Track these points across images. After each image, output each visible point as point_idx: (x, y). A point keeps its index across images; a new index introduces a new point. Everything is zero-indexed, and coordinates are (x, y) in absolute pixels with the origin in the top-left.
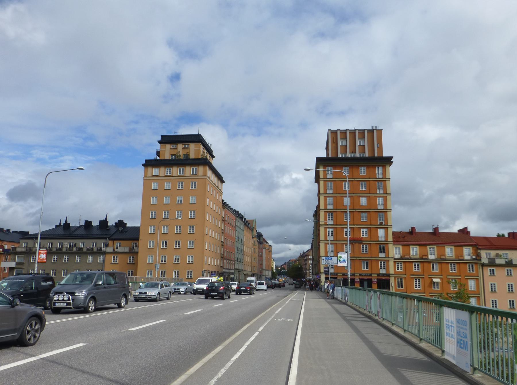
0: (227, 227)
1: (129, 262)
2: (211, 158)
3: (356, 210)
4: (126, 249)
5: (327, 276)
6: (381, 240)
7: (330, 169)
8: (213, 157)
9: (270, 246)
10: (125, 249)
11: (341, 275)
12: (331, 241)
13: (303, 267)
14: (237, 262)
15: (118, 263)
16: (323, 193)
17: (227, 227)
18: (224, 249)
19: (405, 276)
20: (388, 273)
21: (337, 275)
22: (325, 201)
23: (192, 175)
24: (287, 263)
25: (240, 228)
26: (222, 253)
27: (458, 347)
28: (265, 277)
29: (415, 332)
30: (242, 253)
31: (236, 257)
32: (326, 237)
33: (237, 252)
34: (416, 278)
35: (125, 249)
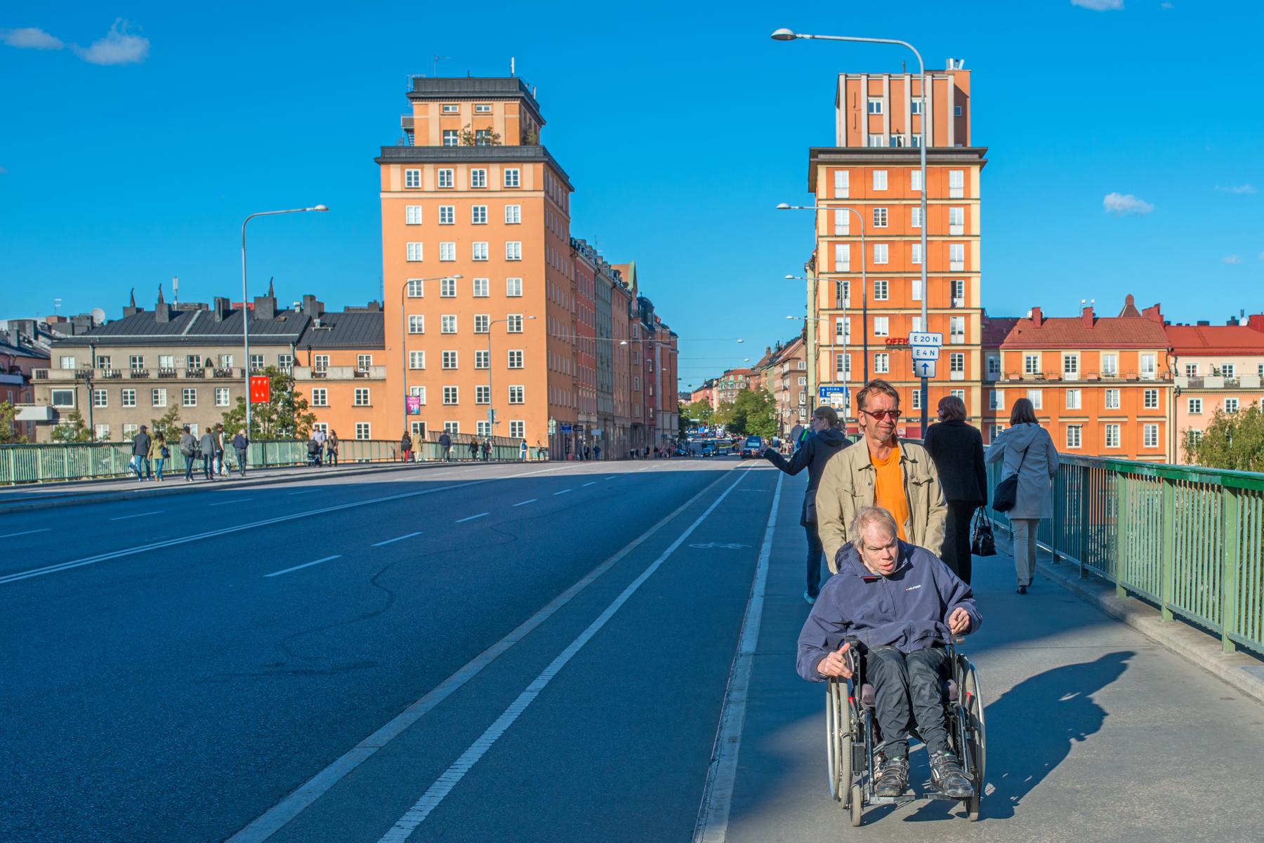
1: (356, 404)
3: (900, 240)
4: (345, 371)
7: (842, 178)
9: (672, 334)
10: (342, 372)
12: (847, 346)
13: (777, 397)
15: (372, 406)
18: (577, 366)
22: (832, 252)
23: (507, 189)
24: (715, 382)
25: (604, 300)
26: (575, 375)
30: (610, 369)
34: (1109, 424)
35: (342, 372)
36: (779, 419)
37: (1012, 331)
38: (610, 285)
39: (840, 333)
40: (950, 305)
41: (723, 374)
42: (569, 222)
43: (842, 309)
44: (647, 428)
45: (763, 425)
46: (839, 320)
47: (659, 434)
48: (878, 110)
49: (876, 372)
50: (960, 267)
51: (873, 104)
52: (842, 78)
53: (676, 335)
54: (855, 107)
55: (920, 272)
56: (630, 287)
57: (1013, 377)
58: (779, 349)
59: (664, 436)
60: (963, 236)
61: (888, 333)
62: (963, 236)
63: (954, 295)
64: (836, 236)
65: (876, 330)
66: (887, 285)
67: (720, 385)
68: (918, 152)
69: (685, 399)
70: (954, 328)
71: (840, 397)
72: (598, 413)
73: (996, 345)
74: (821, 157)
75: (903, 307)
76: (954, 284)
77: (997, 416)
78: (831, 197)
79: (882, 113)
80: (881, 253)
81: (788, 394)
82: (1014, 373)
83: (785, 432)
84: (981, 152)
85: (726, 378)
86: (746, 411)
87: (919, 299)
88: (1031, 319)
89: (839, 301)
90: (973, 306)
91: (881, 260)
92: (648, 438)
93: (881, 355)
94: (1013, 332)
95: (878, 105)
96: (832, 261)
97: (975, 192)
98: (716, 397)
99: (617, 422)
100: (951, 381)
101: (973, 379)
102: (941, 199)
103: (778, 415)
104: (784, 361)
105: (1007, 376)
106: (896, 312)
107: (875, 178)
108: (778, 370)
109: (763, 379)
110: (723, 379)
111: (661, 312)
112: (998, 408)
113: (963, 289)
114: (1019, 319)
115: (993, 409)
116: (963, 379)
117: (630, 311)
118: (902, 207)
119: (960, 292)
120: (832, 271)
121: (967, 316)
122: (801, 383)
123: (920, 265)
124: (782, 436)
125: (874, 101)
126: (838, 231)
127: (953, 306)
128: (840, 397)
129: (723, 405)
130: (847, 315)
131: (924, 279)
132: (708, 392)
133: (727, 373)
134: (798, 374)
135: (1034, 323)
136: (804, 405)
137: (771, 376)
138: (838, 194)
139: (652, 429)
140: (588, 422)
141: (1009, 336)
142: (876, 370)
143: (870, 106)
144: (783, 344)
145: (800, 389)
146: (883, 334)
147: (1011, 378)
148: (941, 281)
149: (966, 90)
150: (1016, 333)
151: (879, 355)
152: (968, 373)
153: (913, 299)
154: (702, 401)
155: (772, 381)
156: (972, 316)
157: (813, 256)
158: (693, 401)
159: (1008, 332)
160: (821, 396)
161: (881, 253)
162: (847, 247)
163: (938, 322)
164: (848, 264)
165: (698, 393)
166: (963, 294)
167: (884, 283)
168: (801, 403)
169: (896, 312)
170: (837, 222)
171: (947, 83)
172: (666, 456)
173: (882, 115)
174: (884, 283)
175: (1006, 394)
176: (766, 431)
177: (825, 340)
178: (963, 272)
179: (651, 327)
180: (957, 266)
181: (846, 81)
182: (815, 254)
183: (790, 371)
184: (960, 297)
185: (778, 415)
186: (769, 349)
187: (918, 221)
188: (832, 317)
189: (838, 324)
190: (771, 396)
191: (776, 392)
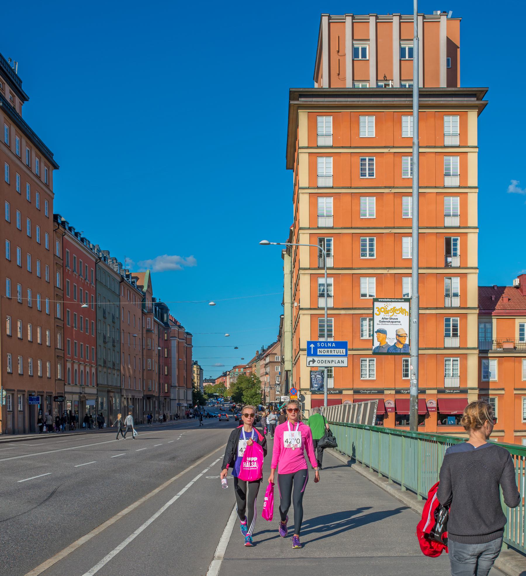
0: (90, 295)
2: (17, 100)
5: (317, 397)
6: (450, 346)
8: (24, 98)
9: (188, 333)
11: (351, 392)
12: (329, 309)
13: (261, 379)
14: (105, 370)
16: (307, 185)
17: (90, 295)
19: (503, 392)
20: (462, 387)
21: (340, 392)
24: (228, 373)
25: (110, 289)
27: (170, 315)
28: (177, 402)
29: (429, 445)
30: (117, 349)
31: (99, 356)
32: (313, 299)
33: (102, 345)
36: (263, 393)
37: (501, 299)
38: (119, 279)
39: (322, 295)
40: (443, 265)
41: (233, 368)
42: (53, 198)
43: (323, 268)
44: (162, 399)
45: (252, 397)
46: (321, 281)
47: (174, 404)
48: (364, 55)
49: (362, 338)
50: (455, 222)
51: (358, 49)
52: (325, 20)
53: (191, 335)
54: (338, 52)
55: (411, 228)
56: (145, 289)
57: (507, 346)
58: (264, 351)
59: (179, 404)
60: (459, 187)
61: (375, 294)
62: (459, 187)
63: (448, 253)
64: (318, 188)
65: (363, 292)
66: (375, 242)
67: (231, 374)
68: (409, 95)
69: (213, 383)
70: (447, 290)
71: (402, 311)
72: (97, 385)
73: (487, 311)
74: (302, 100)
75: (392, 266)
76: (448, 242)
77: (490, 388)
78: (313, 145)
79: (368, 58)
80: (367, 207)
81: (268, 376)
82: (508, 341)
83: (266, 402)
84: (478, 94)
85: (234, 370)
86: (242, 388)
87: (410, 257)
88: (517, 287)
89: (321, 260)
90: (469, 265)
91: (367, 215)
92: (163, 406)
93: (368, 319)
94: (503, 300)
95: (364, 50)
96: (314, 215)
97: (473, 139)
98: (228, 382)
99: (124, 393)
100: (445, 348)
101: (469, 345)
102: (435, 147)
103: (262, 390)
104: (266, 356)
105: (498, 344)
106: (385, 271)
107: (361, 125)
108: (262, 362)
109: (254, 369)
110: (232, 371)
111: (173, 314)
112: (491, 379)
113: (458, 247)
114: (505, 287)
115: (486, 380)
116: (458, 346)
117: (143, 306)
118: (392, 156)
119: (455, 250)
120: (313, 226)
121: (464, 276)
122: (277, 369)
123: (411, 220)
124: (265, 404)
125: (359, 46)
126: (321, 182)
127: (447, 265)
128: (402, 311)
129: (232, 385)
130: (329, 275)
131: (415, 235)
132: (224, 378)
133: (235, 367)
134: (275, 364)
135: (522, 292)
136: (279, 384)
137: (258, 367)
138: (321, 142)
139: (168, 400)
140: (81, 393)
141: (499, 303)
142: (362, 336)
143: (355, 52)
144: (265, 348)
145: (276, 373)
146: (370, 296)
147: (504, 347)
148: (434, 237)
149: (457, 41)
150: (505, 300)
151: (365, 319)
152: (464, 339)
153: (403, 258)
154: (220, 383)
155: (259, 369)
156: (469, 277)
157: (291, 230)
158: (216, 384)
159: (497, 299)
160: (309, 354)
161: (367, 207)
162: (331, 200)
163: (431, 283)
164: (331, 219)
165: (219, 379)
166: (458, 252)
167: (371, 240)
168: (277, 382)
169: (385, 271)
170: (320, 171)
171: (439, 25)
172: (174, 419)
173: (368, 60)
174: (371, 240)
175: (499, 364)
176: (255, 401)
177: (305, 300)
178: (459, 228)
179: (166, 324)
180: (452, 222)
181: (329, 24)
182: (292, 228)
183: (270, 362)
184: (455, 255)
185: (262, 390)
186: (258, 352)
187: (409, 172)
188: (314, 277)
189: (320, 285)
190: (258, 379)
191: (261, 376)
